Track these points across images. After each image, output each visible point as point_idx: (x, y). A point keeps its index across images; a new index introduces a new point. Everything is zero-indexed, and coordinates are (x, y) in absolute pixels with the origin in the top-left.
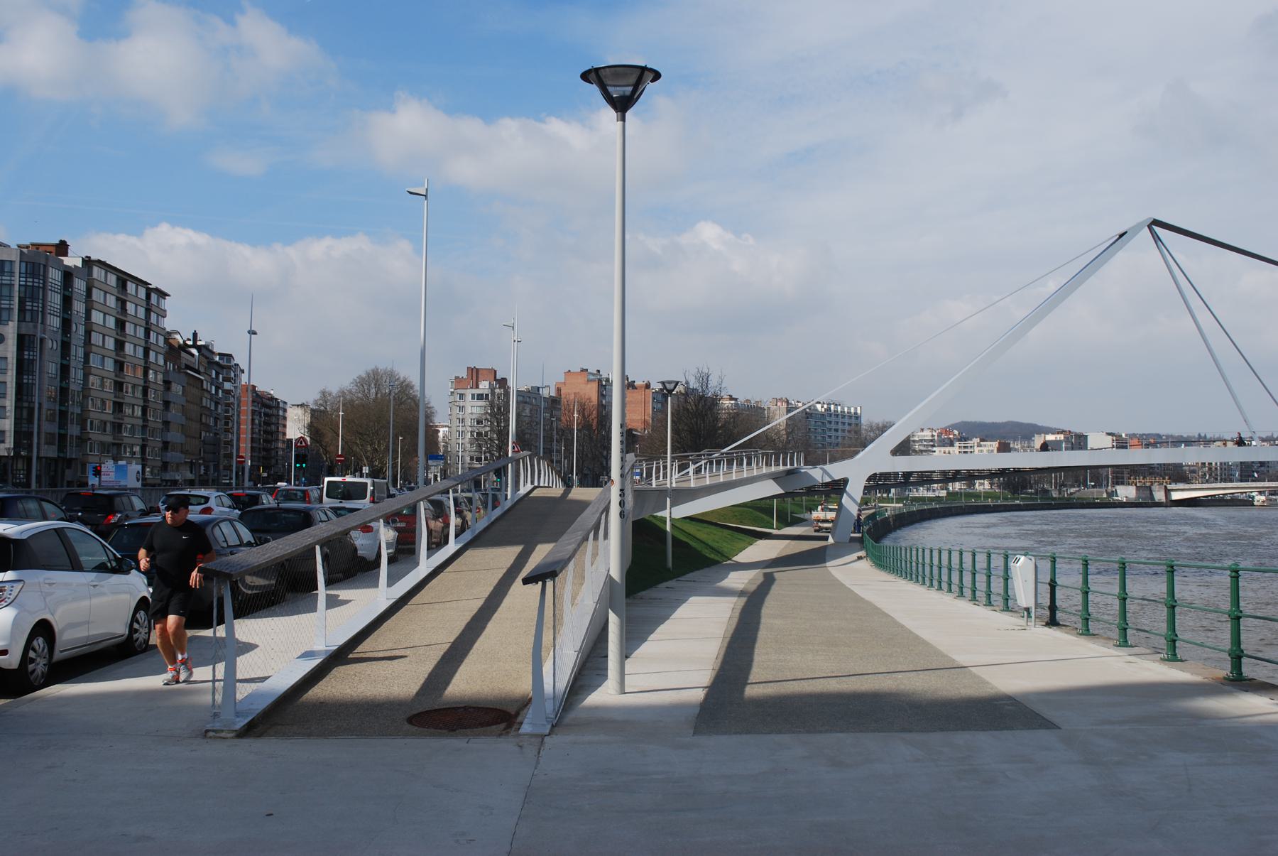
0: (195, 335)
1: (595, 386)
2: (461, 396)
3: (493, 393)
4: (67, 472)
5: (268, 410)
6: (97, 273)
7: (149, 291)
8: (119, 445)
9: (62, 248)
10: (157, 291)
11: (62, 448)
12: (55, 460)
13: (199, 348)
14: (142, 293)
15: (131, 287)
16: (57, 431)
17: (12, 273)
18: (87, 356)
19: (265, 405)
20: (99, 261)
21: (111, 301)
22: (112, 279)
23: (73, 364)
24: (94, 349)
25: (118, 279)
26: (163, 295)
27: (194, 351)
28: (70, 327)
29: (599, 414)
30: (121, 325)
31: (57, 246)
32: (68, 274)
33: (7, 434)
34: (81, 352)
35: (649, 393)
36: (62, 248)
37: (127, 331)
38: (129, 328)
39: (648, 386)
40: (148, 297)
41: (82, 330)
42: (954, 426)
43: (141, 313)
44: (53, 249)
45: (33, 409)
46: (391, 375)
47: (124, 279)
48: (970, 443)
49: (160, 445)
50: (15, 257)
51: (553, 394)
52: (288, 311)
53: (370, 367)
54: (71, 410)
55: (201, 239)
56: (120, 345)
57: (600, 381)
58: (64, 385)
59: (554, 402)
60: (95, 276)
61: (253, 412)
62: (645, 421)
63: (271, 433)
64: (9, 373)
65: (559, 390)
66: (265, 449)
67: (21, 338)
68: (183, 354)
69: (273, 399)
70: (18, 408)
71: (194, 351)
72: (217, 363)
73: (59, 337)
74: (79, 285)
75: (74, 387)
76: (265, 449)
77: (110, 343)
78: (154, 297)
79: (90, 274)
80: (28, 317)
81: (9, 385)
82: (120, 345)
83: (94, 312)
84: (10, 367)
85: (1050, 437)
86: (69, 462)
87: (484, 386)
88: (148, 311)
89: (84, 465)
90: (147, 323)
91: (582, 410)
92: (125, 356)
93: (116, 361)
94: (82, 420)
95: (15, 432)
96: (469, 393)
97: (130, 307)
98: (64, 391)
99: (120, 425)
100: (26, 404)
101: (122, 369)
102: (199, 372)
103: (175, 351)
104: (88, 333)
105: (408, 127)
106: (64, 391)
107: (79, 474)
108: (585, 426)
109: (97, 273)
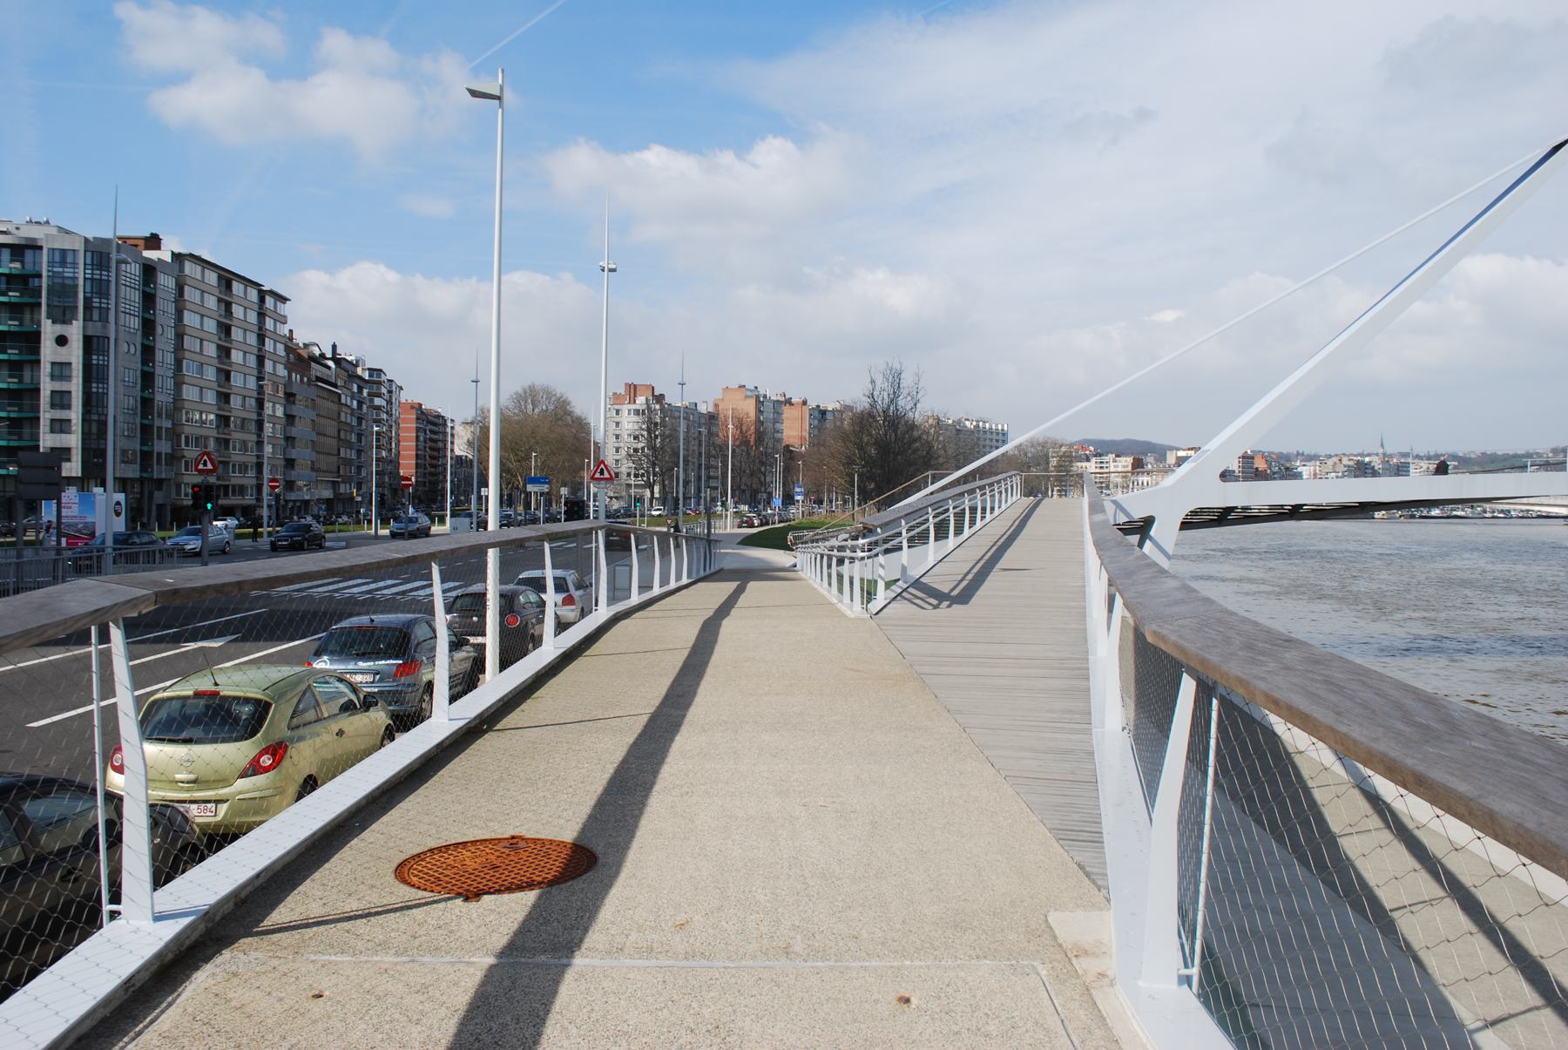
0: (334, 347)
1: (753, 402)
2: (618, 412)
3: (649, 408)
4: (157, 494)
5: (432, 427)
6: (189, 268)
7: (262, 295)
8: (226, 463)
9: (154, 242)
10: (273, 293)
11: (144, 468)
12: (141, 480)
13: (338, 361)
14: (253, 295)
15: (237, 288)
16: (138, 447)
17: (75, 265)
18: (178, 363)
19: (429, 422)
20: (191, 255)
21: (211, 302)
22: (212, 278)
23: (158, 371)
24: (187, 355)
25: (220, 277)
26: (284, 300)
27: (331, 363)
28: (154, 329)
29: (757, 430)
30: (225, 329)
31: (146, 239)
32: (149, 270)
33: (74, 452)
34: (170, 358)
35: (806, 409)
36: (154, 242)
37: (234, 336)
38: (237, 334)
39: (805, 403)
40: (262, 300)
41: (171, 334)
42: (1091, 442)
43: (253, 317)
44: (141, 243)
45: (105, 423)
46: (549, 394)
47: (227, 279)
48: (1105, 459)
49: (282, 463)
50: (79, 246)
51: (711, 409)
52: (441, 325)
53: (526, 384)
54: (157, 423)
55: (392, 276)
56: (224, 352)
57: (758, 397)
58: (146, 394)
59: (712, 417)
60: (187, 271)
61: (418, 430)
62: (801, 437)
63: (438, 450)
64: (74, 381)
65: (716, 405)
66: (432, 466)
67: (88, 341)
68: (313, 365)
69: (439, 416)
70: (86, 420)
71: (331, 363)
72: (361, 378)
73: (139, 339)
74: (166, 282)
75: (162, 398)
76: (432, 466)
77: (211, 350)
78: (269, 301)
79: (182, 269)
80: (96, 316)
81: (74, 394)
82: (224, 352)
83: (186, 313)
84: (74, 373)
85: (1181, 454)
86: (159, 483)
87: (641, 400)
88: (262, 315)
89: (178, 486)
90: (260, 329)
91: (739, 424)
92: (231, 364)
93: (219, 370)
94: (174, 434)
95: (83, 449)
96: (625, 408)
97: (238, 311)
98: (147, 404)
99: (227, 442)
100: (95, 417)
101: (228, 378)
102: (335, 386)
103: (301, 360)
104: (180, 337)
105: (579, 165)
106: (147, 404)
107: (173, 495)
108: (743, 441)
109: (189, 268)
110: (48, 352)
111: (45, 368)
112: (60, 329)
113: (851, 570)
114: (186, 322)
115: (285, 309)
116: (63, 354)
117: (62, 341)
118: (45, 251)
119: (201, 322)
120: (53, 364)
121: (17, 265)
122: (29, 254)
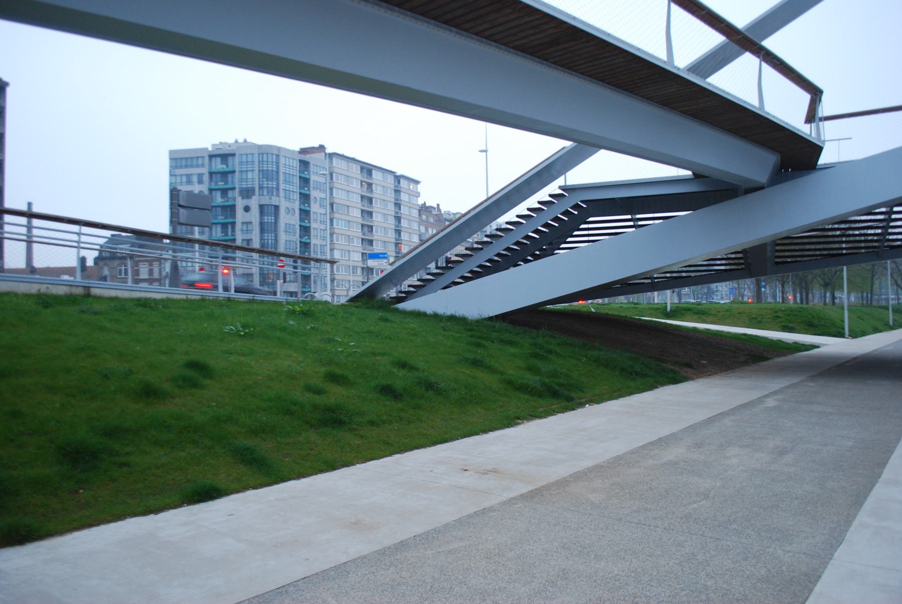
22: (355, 170)
26: (417, 182)
47: (367, 169)
60: (334, 164)
64: (254, 232)
110: (240, 216)
111: (238, 226)
112: (246, 202)
113: (289, 265)
114: (334, 195)
115: (420, 188)
116: (248, 217)
117: (247, 209)
118: (237, 156)
119: (348, 194)
120: (243, 223)
121: (224, 166)
122: (230, 159)
